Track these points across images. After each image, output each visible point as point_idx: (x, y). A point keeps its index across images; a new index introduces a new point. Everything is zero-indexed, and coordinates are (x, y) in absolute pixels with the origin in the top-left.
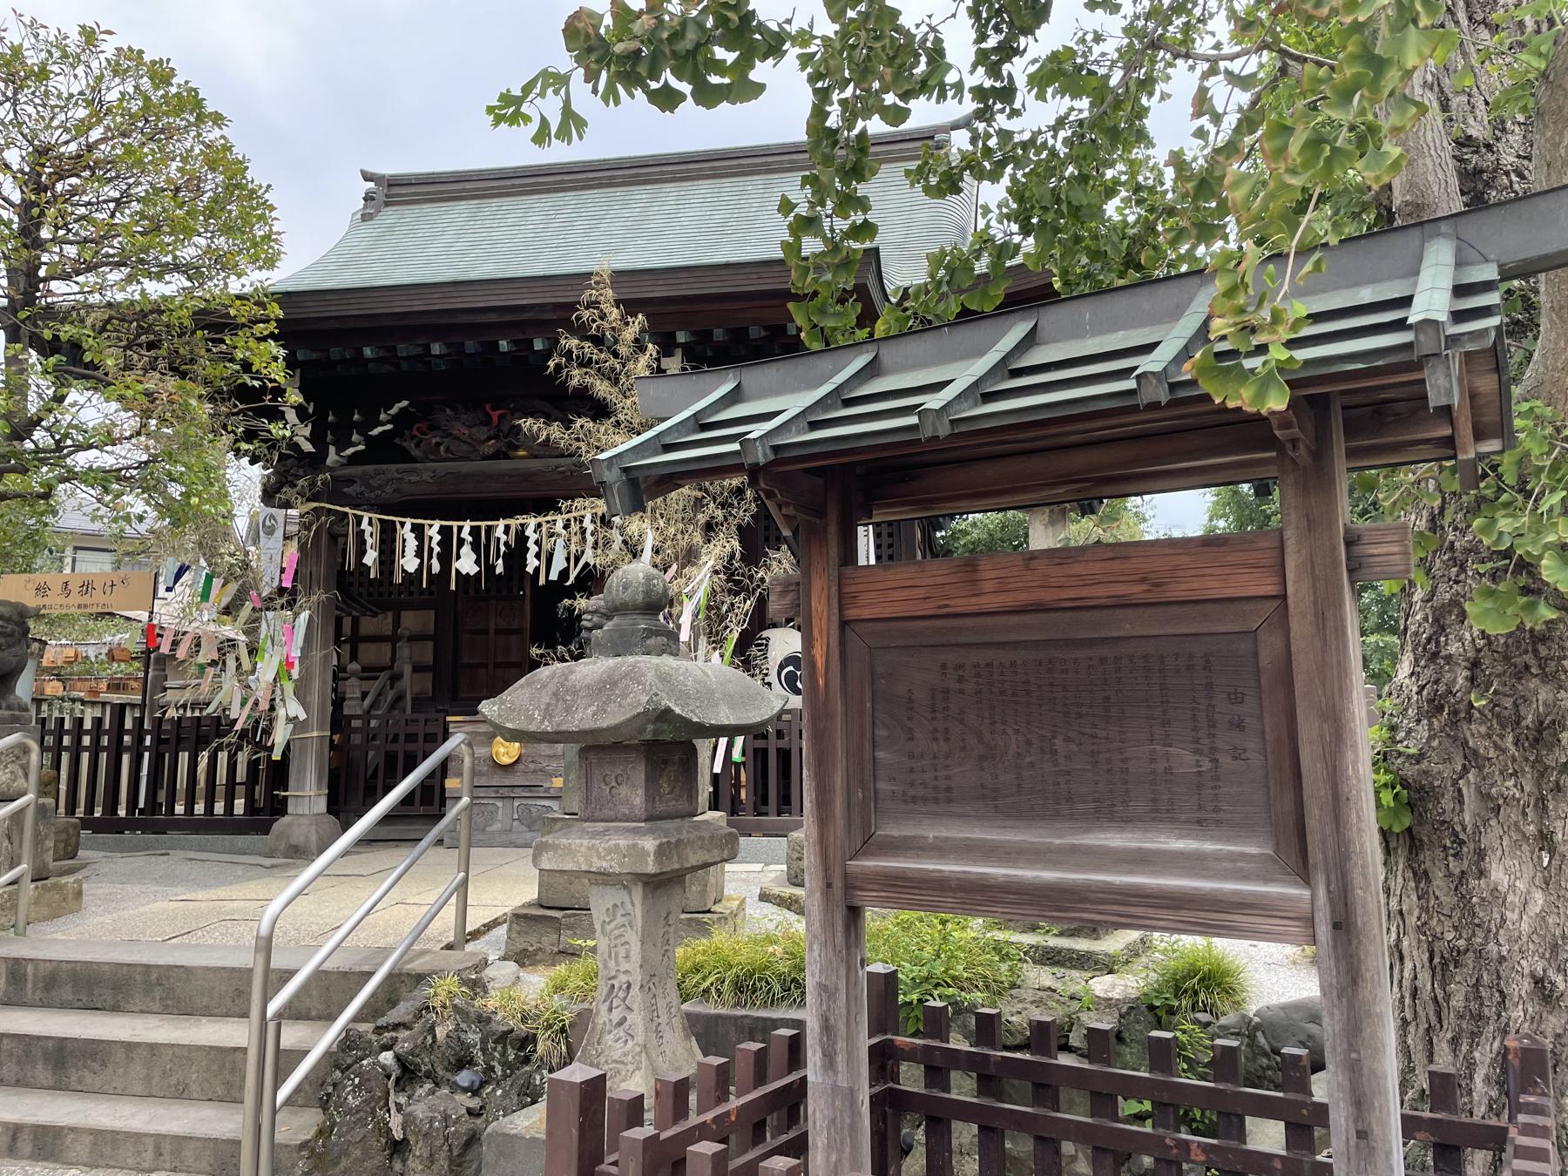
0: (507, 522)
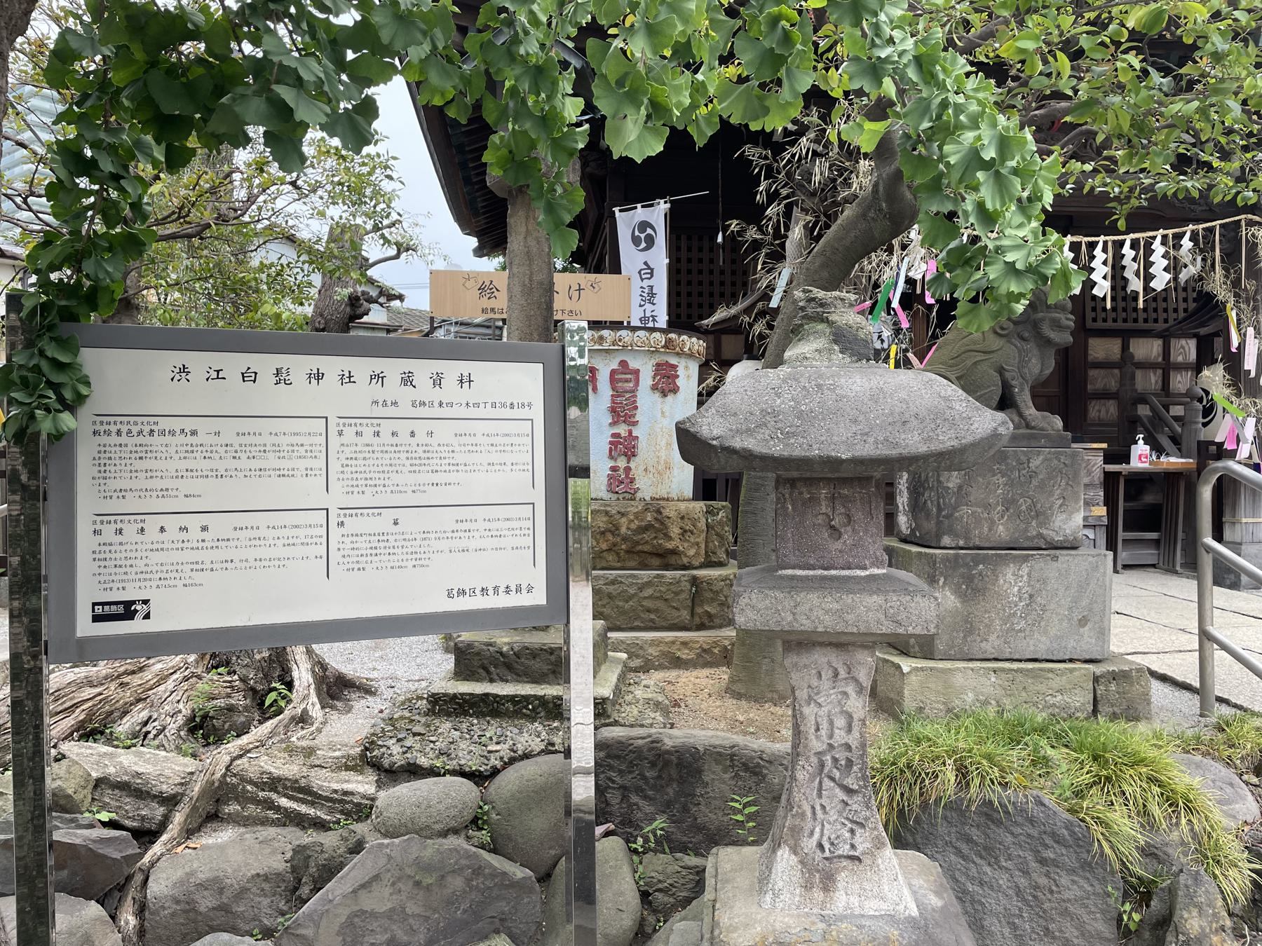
0: (1076, 239)
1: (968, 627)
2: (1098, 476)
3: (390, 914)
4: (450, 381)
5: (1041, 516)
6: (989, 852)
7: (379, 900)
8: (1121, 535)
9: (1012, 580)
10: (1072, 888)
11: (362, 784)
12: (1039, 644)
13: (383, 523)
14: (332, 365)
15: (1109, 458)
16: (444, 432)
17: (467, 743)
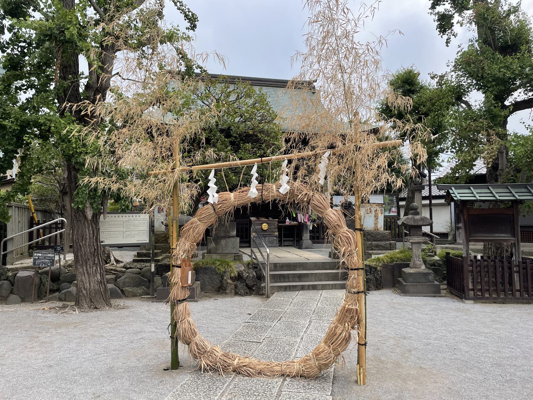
1: (216, 249)
2: (276, 226)
3: (128, 282)
4: (137, 216)
5: (229, 232)
6: (206, 273)
7: (127, 280)
8: (283, 239)
9: (223, 242)
10: (215, 277)
11: (124, 269)
12: (227, 251)
13: (130, 233)
14: (124, 215)
15: (279, 222)
16: (137, 222)
17: (138, 265)
